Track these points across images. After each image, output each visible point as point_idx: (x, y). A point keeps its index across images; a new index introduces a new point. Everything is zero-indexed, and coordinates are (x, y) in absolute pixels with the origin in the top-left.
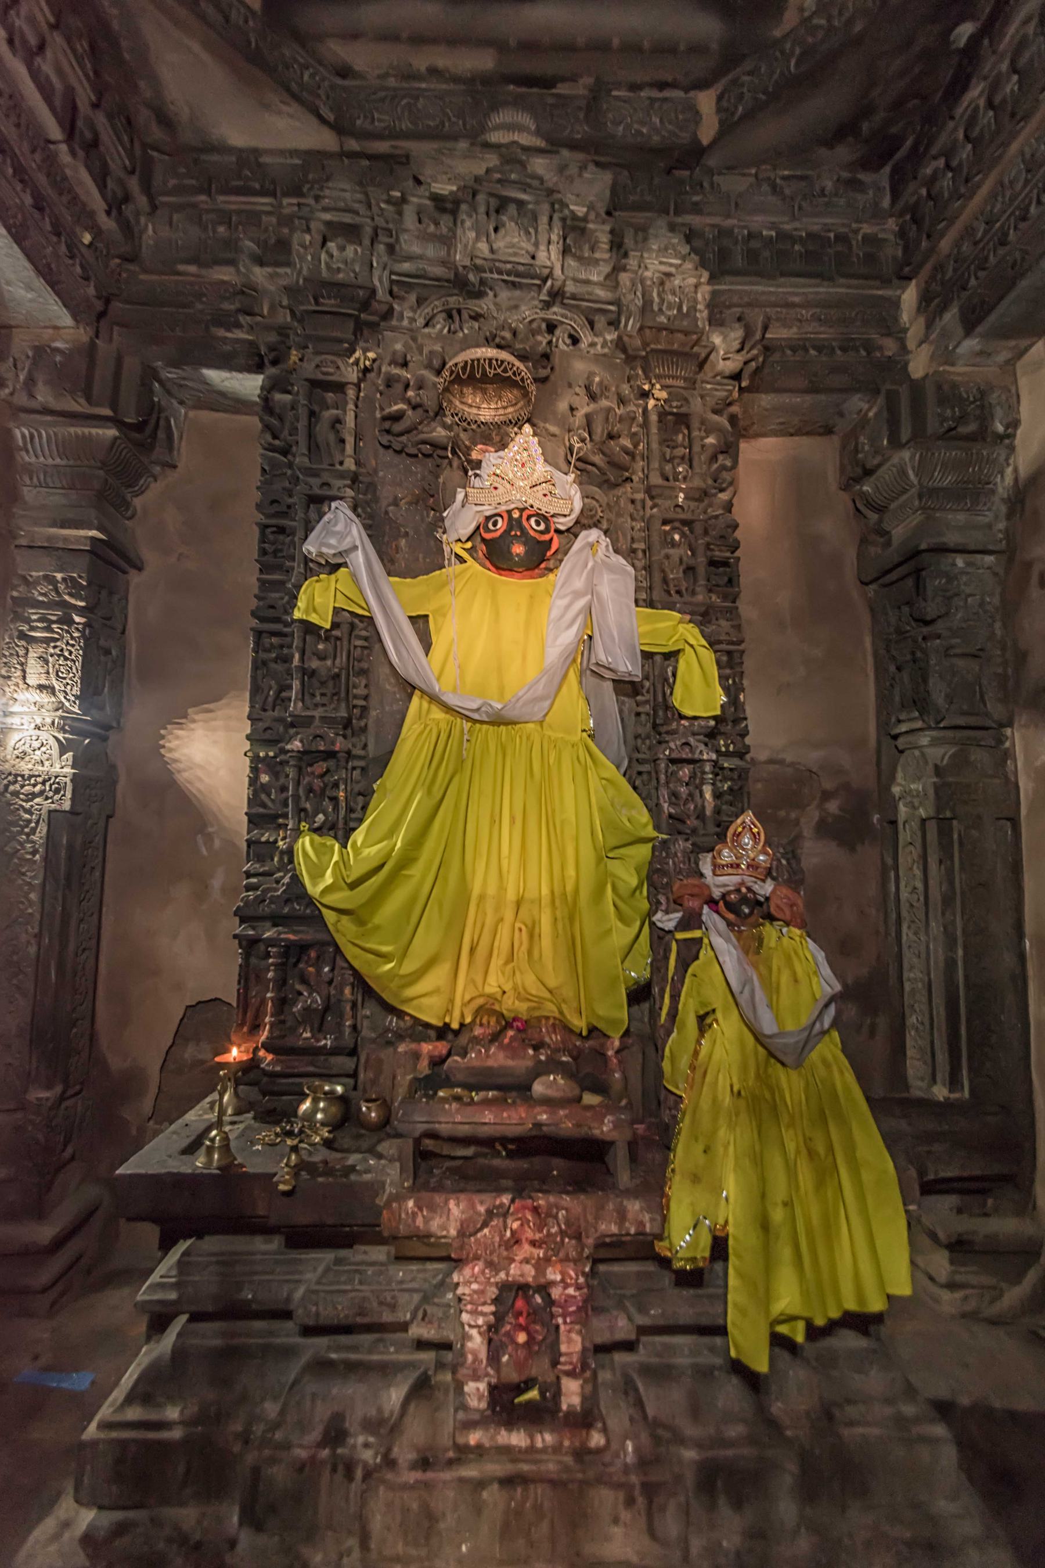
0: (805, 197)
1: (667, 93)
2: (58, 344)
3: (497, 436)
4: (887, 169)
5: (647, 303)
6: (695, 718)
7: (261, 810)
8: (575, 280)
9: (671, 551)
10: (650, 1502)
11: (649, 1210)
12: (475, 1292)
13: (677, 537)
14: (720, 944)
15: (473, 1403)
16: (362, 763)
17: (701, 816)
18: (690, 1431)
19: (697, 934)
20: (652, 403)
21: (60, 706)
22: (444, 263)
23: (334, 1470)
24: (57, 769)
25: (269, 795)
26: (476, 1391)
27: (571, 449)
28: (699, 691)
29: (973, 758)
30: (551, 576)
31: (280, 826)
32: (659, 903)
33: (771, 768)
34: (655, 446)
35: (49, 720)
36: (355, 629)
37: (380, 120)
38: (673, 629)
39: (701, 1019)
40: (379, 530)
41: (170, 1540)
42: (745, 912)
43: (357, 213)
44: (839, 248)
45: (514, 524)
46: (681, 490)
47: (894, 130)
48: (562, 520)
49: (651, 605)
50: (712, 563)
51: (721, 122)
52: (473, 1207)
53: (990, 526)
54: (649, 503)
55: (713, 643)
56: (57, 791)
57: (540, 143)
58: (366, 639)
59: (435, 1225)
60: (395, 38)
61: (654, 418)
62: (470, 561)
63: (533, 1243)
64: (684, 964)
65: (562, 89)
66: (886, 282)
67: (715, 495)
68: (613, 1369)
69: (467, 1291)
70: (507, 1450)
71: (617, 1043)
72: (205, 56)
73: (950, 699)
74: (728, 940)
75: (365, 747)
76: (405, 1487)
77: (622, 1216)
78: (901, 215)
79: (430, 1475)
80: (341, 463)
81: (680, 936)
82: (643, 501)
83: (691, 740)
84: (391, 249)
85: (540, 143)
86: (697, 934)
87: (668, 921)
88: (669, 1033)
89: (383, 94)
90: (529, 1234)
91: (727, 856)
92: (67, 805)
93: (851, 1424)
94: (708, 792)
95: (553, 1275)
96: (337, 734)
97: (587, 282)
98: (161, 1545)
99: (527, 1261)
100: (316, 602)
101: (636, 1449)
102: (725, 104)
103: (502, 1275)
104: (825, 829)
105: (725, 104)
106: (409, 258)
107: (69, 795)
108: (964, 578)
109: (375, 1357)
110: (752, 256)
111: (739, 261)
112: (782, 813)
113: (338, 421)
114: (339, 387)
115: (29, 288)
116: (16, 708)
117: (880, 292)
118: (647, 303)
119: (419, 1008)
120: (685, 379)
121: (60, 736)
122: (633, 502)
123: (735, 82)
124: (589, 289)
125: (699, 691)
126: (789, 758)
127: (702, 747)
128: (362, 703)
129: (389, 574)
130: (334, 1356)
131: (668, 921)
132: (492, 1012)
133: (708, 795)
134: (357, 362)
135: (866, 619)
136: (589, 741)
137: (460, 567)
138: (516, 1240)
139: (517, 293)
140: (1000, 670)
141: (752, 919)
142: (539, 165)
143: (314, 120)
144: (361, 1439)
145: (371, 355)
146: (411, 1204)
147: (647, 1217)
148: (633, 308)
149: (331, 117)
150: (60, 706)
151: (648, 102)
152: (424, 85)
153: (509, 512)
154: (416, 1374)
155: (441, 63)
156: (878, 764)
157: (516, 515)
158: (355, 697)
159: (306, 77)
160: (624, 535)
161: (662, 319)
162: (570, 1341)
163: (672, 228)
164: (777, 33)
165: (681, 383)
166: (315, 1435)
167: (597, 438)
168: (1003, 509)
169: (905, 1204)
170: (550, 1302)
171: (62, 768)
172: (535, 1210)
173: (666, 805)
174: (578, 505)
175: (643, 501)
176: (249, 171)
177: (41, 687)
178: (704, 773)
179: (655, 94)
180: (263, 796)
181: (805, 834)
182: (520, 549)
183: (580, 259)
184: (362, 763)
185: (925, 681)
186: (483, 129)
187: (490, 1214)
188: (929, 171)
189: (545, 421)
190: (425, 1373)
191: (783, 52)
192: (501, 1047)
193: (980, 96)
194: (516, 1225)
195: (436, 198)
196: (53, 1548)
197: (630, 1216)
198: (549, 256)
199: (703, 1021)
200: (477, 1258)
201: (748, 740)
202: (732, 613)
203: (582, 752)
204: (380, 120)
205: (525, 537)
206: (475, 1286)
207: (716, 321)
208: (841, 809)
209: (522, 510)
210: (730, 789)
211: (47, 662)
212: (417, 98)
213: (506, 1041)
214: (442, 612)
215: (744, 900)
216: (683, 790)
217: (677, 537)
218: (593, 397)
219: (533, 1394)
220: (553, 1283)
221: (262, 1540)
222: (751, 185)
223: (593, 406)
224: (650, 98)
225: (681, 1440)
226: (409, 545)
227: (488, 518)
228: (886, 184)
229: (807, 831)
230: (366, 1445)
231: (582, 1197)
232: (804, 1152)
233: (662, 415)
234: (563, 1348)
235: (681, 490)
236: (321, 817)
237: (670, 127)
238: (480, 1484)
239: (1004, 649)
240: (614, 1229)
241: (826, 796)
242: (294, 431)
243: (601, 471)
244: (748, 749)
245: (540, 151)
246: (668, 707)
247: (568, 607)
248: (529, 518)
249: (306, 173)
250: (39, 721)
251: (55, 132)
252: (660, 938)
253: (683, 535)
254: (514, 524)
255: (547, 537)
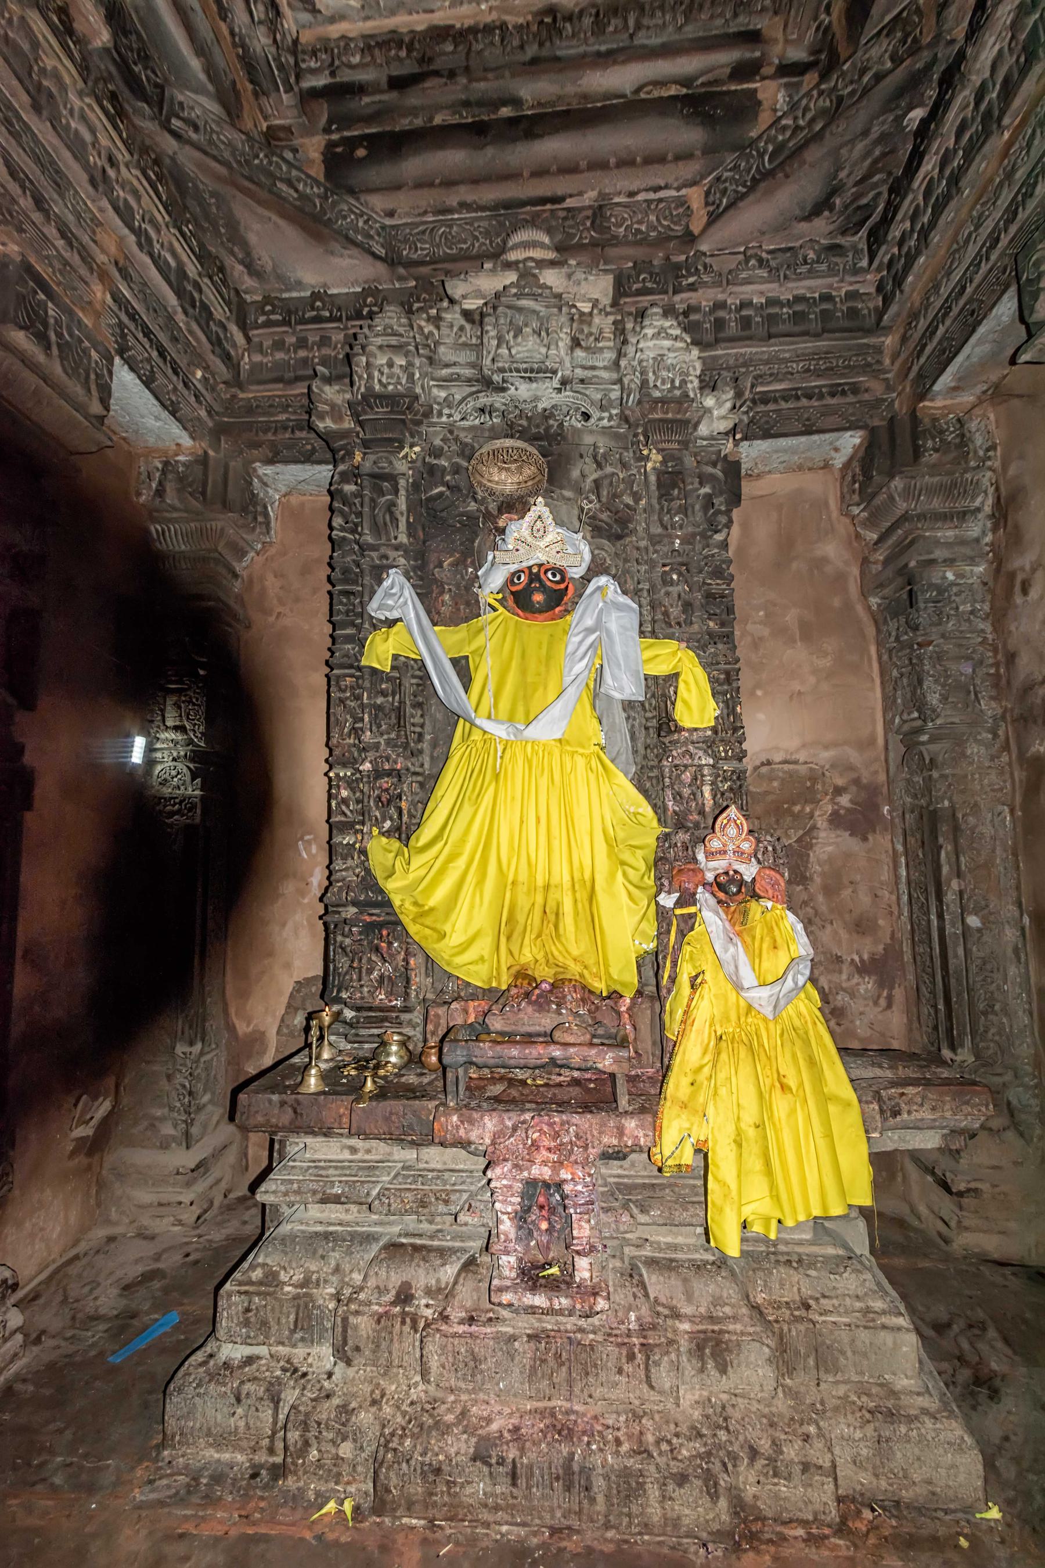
0: (789, 267)
1: (662, 194)
2: (181, 458)
3: (516, 505)
4: (863, 232)
5: (644, 383)
6: (696, 729)
7: (343, 819)
8: (584, 368)
9: (671, 589)
10: (648, 1358)
11: (642, 1127)
12: (505, 1186)
13: (675, 577)
14: (711, 918)
15: (506, 1272)
16: (420, 779)
17: (702, 812)
18: (687, 1310)
19: (692, 910)
20: (650, 465)
21: (190, 742)
22: (472, 365)
23: (403, 1323)
24: (190, 792)
25: (348, 807)
26: (508, 1263)
27: (582, 509)
28: (696, 707)
29: (969, 752)
30: (568, 617)
31: (356, 832)
32: (662, 885)
33: (786, 767)
34: (654, 502)
35: (182, 753)
36: (410, 671)
37: (422, 249)
38: (670, 656)
39: (693, 980)
40: (427, 591)
41: (284, 1370)
42: (732, 891)
43: (401, 335)
44: (825, 306)
45: (534, 577)
46: (678, 537)
47: (864, 201)
48: (574, 570)
49: (654, 634)
50: (709, 596)
51: (710, 214)
52: (502, 1122)
53: (977, 540)
54: (651, 549)
55: (707, 666)
56: (190, 810)
57: (551, 255)
58: (421, 678)
59: (473, 1136)
60: (431, 185)
61: (653, 478)
62: (501, 609)
63: (549, 1150)
64: (682, 934)
65: (569, 203)
66: (868, 332)
67: (711, 537)
68: (622, 1260)
69: (498, 1185)
70: (532, 1310)
71: (628, 1001)
72: (281, 222)
73: (944, 699)
74: (717, 914)
75: (422, 765)
76: (455, 1335)
77: (621, 1132)
78: (879, 270)
79: (474, 1328)
80: (396, 538)
81: (678, 912)
82: (646, 549)
83: (691, 748)
84: (431, 361)
85: (551, 255)
86: (692, 910)
87: (668, 901)
88: (669, 991)
89: (421, 228)
90: (546, 1143)
91: (715, 844)
92: (198, 820)
93: (825, 1313)
94: (707, 790)
95: (565, 1175)
96: (398, 755)
97: (593, 368)
98: (278, 1373)
99: (544, 1163)
100: (381, 651)
101: (638, 1319)
102: (711, 199)
103: (526, 1174)
104: (836, 820)
105: (711, 199)
106: (447, 366)
107: (199, 811)
108: (955, 589)
109: (436, 1243)
110: (746, 323)
111: (733, 328)
112: (797, 808)
113: (393, 504)
114: (392, 478)
115: (157, 418)
116: (158, 746)
117: (865, 341)
118: (644, 383)
119: (468, 974)
120: (679, 442)
121: (191, 766)
122: (638, 549)
123: (718, 179)
124: (595, 373)
125: (696, 707)
126: (802, 757)
127: (701, 753)
128: (418, 729)
129: (435, 624)
130: (404, 1240)
131: (668, 901)
132: (526, 976)
133: (707, 794)
134: (406, 456)
135: (871, 631)
136: (601, 753)
137: (494, 614)
138: (535, 1146)
139: (534, 385)
140: (992, 671)
141: (740, 897)
142: (551, 278)
143: (370, 259)
144: (423, 1302)
145: (417, 449)
146: (455, 1118)
147: (641, 1134)
148: (633, 386)
149: (382, 252)
150: (190, 742)
151: (644, 205)
152: (456, 216)
153: (530, 568)
154: (465, 1257)
155: (469, 198)
156: (886, 761)
157: (535, 570)
158: (414, 725)
159: (361, 224)
160: (632, 578)
161: (657, 394)
162: (580, 1227)
163: (669, 311)
164: (754, 134)
165: (676, 446)
166: (390, 1297)
167: (604, 500)
168: (989, 524)
169: (867, 1131)
170: (564, 1197)
171: (193, 791)
172: (551, 1125)
173: (671, 804)
174: (587, 557)
175: (646, 549)
176: (321, 308)
177: (176, 728)
178: (703, 776)
179: (652, 196)
180: (344, 808)
181: (819, 825)
182: (542, 595)
183: (587, 349)
184: (420, 779)
185: (920, 682)
186: (503, 249)
187: (515, 1129)
188: (898, 234)
189: (561, 488)
190: (473, 1256)
191: (758, 151)
192: (530, 1003)
193: (933, 169)
194: (536, 1135)
195: (467, 314)
196: (202, 1370)
197: (627, 1132)
198: (560, 353)
199: (694, 983)
200: (505, 1160)
201: (744, 746)
202: (728, 638)
203: (594, 762)
204: (422, 249)
205: (543, 588)
206: (505, 1182)
207: (709, 385)
208: (851, 801)
209: (540, 565)
210: (731, 789)
211: (180, 708)
212: (451, 227)
213: (534, 998)
214: (480, 652)
215: (732, 881)
216: (686, 792)
217: (675, 577)
218: (599, 466)
219: (554, 1270)
220: (565, 1181)
221: (351, 1372)
222: (740, 263)
223: (600, 473)
224: (646, 201)
225: (676, 1315)
226: (450, 601)
227: (513, 574)
228: (863, 246)
229: (821, 823)
230: (427, 1306)
231: (589, 1116)
232: (777, 1085)
233: (660, 474)
234: (575, 1233)
235: (678, 537)
236: (388, 824)
237: (666, 223)
238: (513, 1338)
239: (995, 651)
240: (615, 1142)
241: (838, 791)
242: (360, 514)
243: (609, 528)
244: (744, 753)
245: (552, 264)
246: (670, 719)
247: (581, 643)
248: (546, 572)
249: (361, 309)
250: (175, 754)
251: (172, 300)
252: (663, 915)
253: (680, 574)
254: (534, 577)
255: (562, 586)
